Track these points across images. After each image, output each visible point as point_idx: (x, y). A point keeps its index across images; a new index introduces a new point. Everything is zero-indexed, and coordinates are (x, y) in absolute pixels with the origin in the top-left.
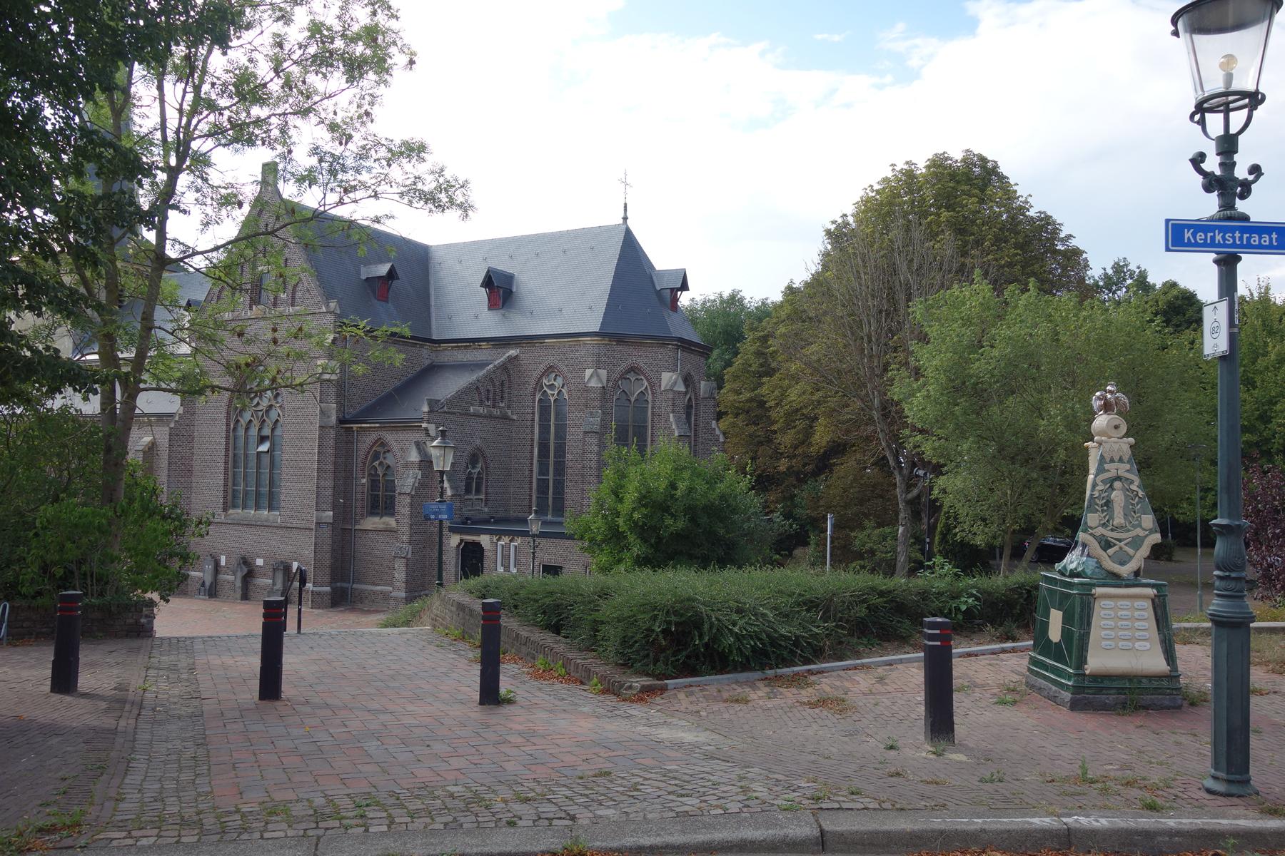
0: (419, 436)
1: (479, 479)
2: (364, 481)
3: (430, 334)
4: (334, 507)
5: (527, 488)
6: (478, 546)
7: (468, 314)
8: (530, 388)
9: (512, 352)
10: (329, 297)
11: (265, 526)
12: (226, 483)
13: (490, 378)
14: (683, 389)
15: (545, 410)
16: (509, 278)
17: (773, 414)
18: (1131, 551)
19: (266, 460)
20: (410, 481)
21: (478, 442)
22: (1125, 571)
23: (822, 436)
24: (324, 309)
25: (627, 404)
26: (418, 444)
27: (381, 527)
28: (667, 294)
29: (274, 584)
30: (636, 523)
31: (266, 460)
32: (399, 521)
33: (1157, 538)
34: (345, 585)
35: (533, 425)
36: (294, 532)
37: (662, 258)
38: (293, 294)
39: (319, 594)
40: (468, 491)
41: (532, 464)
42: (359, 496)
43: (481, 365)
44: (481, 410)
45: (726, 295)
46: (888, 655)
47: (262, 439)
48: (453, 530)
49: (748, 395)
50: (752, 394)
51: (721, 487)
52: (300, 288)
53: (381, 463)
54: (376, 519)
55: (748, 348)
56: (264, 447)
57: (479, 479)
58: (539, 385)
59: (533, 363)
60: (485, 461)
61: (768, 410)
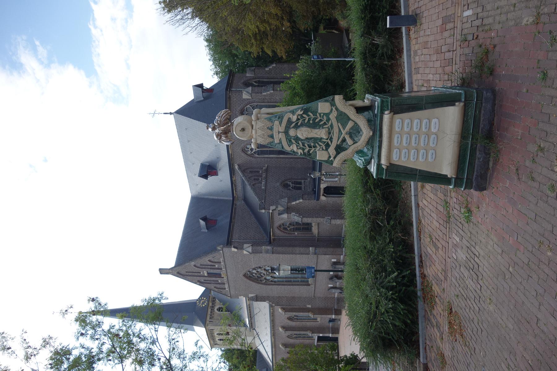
2: (296, 233)
4: (308, 246)
6: (325, 189)
7: (221, 181)
9: (236, 167)
10: (214, 250)
12: (298, 285)
13: (249, 179)
14: (250, 88)
15: (262, 153)
16: (203, 166)
18: (350, 125)
20: (296, 217)
21: (278, 184)
22: (366, 133)
26: (279, 214)
27: (316, 227)
32: (314, 222)
33: (338, 98)
35: (269, 158)
36: (319, 261)
37: (188, 96)
38: (215, 262)
40: (300, 188)
41: (288, 158)
42: (302, 235)
44: (263, 183)
45: (206, 44)
46: (413, 233)
48: (318, 199)
49: (253, 41)
50: (253, 38)
51: (298, 88)
53: (288, 227)
54: (313, 228)
59: (241, 158)
60: (287, 180)
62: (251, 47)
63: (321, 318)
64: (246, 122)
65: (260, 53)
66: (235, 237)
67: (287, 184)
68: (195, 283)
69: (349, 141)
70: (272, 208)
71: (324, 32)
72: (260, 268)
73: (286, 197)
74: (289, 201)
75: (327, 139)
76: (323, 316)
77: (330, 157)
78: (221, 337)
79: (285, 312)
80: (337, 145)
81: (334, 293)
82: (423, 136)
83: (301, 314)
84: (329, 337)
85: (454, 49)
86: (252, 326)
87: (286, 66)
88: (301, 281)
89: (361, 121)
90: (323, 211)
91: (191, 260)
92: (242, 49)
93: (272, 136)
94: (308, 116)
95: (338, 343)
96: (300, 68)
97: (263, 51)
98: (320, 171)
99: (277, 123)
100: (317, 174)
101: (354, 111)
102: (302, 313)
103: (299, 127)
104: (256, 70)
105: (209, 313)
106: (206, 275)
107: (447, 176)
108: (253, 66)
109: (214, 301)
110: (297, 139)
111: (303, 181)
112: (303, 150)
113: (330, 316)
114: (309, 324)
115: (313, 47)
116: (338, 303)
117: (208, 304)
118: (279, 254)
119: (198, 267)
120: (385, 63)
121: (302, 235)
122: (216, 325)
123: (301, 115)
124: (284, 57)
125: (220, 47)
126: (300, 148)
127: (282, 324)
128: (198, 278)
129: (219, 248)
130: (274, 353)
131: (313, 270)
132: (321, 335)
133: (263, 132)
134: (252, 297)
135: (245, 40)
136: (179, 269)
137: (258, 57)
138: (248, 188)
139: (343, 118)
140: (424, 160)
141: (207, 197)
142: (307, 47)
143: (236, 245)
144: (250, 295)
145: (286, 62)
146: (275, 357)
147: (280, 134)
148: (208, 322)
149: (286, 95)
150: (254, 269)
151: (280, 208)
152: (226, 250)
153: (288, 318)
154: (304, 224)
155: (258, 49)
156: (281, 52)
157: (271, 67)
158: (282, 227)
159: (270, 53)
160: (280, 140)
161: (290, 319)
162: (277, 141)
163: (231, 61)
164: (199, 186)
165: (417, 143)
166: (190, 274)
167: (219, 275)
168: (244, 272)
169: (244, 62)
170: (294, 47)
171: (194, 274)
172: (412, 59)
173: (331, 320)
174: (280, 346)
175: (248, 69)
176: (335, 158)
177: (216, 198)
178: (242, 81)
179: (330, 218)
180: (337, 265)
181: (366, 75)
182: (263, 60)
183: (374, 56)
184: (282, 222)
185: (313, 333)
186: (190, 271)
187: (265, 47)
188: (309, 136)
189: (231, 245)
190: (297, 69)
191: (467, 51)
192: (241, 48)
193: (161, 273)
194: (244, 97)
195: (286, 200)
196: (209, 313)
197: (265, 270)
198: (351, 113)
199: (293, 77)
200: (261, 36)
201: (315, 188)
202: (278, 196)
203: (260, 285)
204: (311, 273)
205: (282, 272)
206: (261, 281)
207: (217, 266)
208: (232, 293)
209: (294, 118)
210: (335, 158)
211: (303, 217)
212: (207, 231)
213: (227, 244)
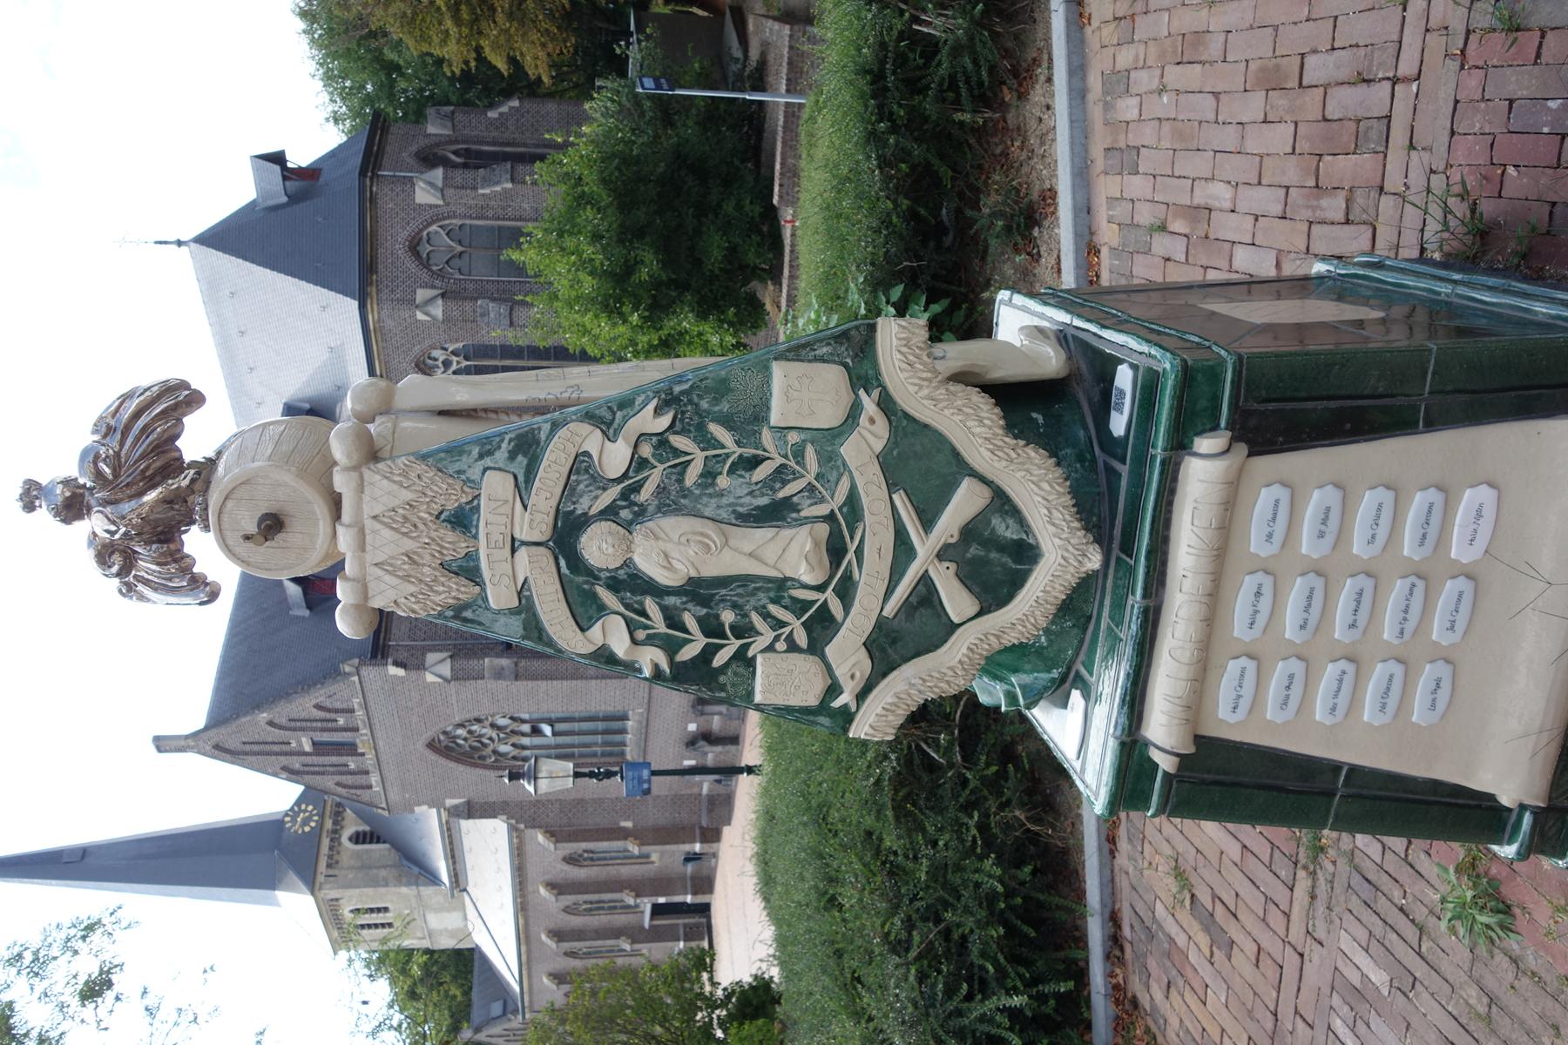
11: (646, 726)
18: (965, 502)
19: (560, 727)
22: (1062, 554)
24: (356, 678)
25: (466, 257)
28: (293, 185)
29: (720, 713)
30: (645, 319)
31: (560, 727)
37: (237, 190)
38: (337, 711)
45: (301, 25)
47: (536, 731)
49: (449, 23)
52: (328, 704)
56: (547, 729)
62: (444, 42)
63: (662, 854)
64: (288, 478)
65: (473, 64)
68: (275, 775)
69: (956, 600)
71: (666, 10)
72: (478, 720)
75: (821, 588)
76: (668, 847)
77: (833, 690)
79: (557, 842)
80: (881, 624)
81: (700, 785)
82: (1400, 587)
84: (684, 904)
85: (1407, 67)
87: (551, 107)
88: (603, 754)
89: (1038, 490)
91: (258, 707)
92: (413, 48)
93: (469, 570)
94: (708, 442)
95: (709, 918)
96: (598, 115)
97: (480, 58)
99: (497, 485)
101: (987, 411)
103: (641, 513)
104: (459, 117)
105: (325, 849)
106: (308, 748)
107: (1491, 797)
108: (448, 103)
109: (338, 814)
110: (631, 583)
112: (671, 647)
113: (687, 847)
114: (627, 871)
115: (634, 54)
116: (710, 811)
117: (321, 824)
118: (536, 679)
119: (281, 727)
120: (958, 116)
122: (349, 885)
123: (662, 442)
124: (545, 79)
126: (651, 640)
127: (547, 877)
128: (284, 760)
129: (347, 669)
130: (524, 958)
131: (646, 773)
132: (662, 900)
133: (409, 545)
134: (456, 807)
135: (423, 20)
136: (225, 735)
137: (466, 74)
139: (922, 466)
140: (1386, 718)
142: (618, 51)
143: (402, 655)
144: (450, 802)
145: (550, 95)
146: (529, 969)
147: (523, 553)
148: (320, 878)
149: (554, 198)
152: (370, 672)
155: (464, 49)
156: (537, 64)
157: (505, 109)
159: (501, 64)
160: (523, 592)
161: (571, 860)
162: (500, 596)
163: (382, 85)
165: (1362, 623)
166: (256, 748)
167: (350, 749)
168: (428, 735)
169: (422, 90)
170: (576, 52)
172: (1096, 112)
173: (691, 858)
174: (543, 937)
175: (430, 111)
176: (861, 696)
178: (414, 148)
181: (883, 163)
182: (481, 85)
183: (914, 86)
185: (638, 896)
187: (484, 43)
188: (711, 569)
189: (385, 656)
190: (587, 119)
191: (1519, 82)
192: (410, 42)
194: (418, 200)
196: (325, 849)
197: (493, 726)
198: (973, 428)
199: (572, 144)
203: (479, 771)
204: (641, 781)
205: (544, 785)
206: (482, 758)
207: (341, 721)
209: (615, 457)
210: (861, 696)
212: (307, 613)
213: (374, 656)
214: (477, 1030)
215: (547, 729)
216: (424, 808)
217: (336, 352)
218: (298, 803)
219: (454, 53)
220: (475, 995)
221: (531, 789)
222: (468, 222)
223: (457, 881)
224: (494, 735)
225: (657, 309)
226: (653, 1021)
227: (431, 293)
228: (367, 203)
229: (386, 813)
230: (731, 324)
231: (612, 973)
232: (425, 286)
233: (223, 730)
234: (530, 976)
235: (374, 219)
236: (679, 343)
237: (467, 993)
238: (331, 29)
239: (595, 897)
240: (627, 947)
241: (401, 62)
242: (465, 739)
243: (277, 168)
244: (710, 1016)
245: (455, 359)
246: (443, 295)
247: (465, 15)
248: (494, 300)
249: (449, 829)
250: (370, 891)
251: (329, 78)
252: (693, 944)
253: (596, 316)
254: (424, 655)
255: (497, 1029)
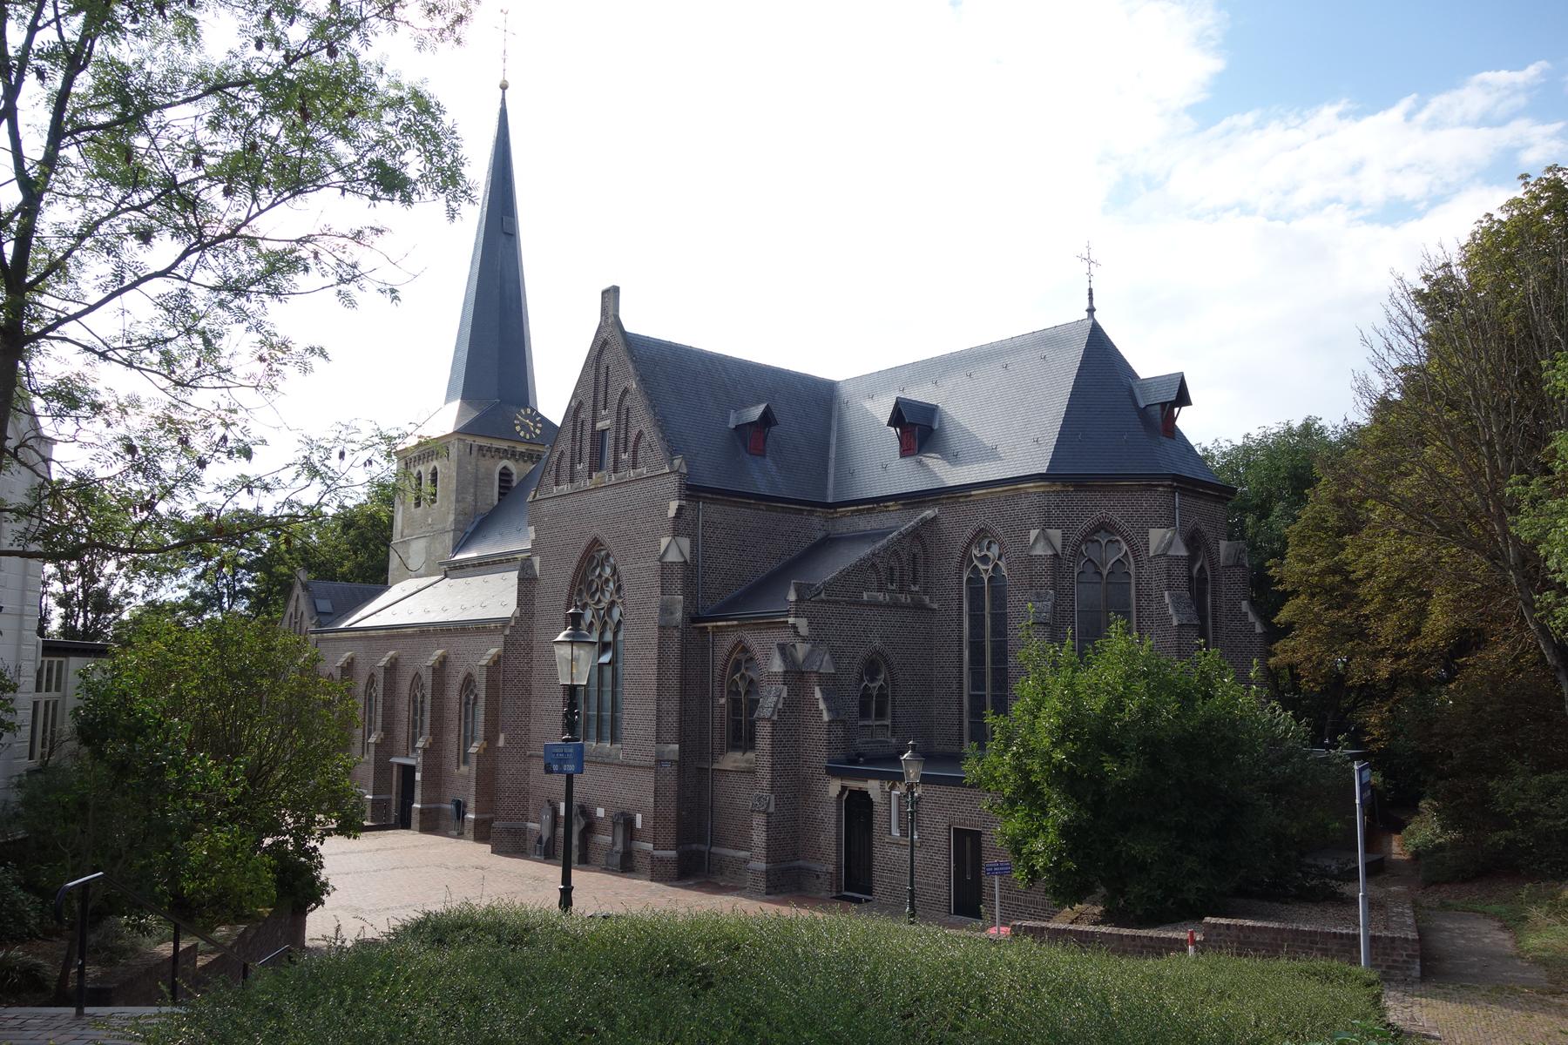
0: (784, 636)
1: (882, 696)
2: (723, 701)
3: (826, 497)
5: (955, 709)
7: (882, 467)
8: (954, 563)
9: (929, 513)
10: (672, 451)
14: (1183, 552)
16: (930, 411)
17: (1362, 591)
19: (608, 672)
21: (877, 643)
23: (1439, 620)
25: (1096, 579)
26: (782, 648)
29: (614, 843)
31: (608, 672)
32: (760, 757)
34: (702, 847)
35: (960, 614)
38: (635, 452)
39: (661, 860)
40: (864, 714)
41: (961, 672)
42: (717, 720)
43: (883, 535)
44: (880, 597)
45: (1297, 424)
48: (833, 772)
49: (1321, 564)
52: (643, 444)
54: (738, 755)
55: (1321, 495)
56: (606, 658)
57: (882, 696)
58: (966, 557)
59: (957, 526)
61: (1356, 584)
62: (1302, 559)
63: (467, 777)
65: (1280, 588)
66: (713, 512)
67: (878, 672)
68: (575, 395)
70: (803, 625)
73: (838, 669)
74: (823, 680)
76: (473, 784)
78: (426, 479)
81: (539, 821)
83: (481, 717)
86: (455, 570)
90: (792, 787)
91: (643, 380)
97: (1285, 597)
98: (925, 780)
100: (913, 772)
102: (482, 718)
105: (497, 444)
106: (599, 425)
111: (888, 722)
113: (471, 804)
114: (452, 739)
116: (508, 831)
117: (522, 441)
119: (621, 401)
121: (717, 720)
122: (460, 466)
125: (1295, 462)
128: (589, 404)
129: (677, 462)
130: (373, 633)
131: (571, 768)
132: (418, 776)
134: (532, 566)
135: (1321, 539)
136: (618, 345)
138: (865, 551)
141: (835, 428)
143: (688, 514)
144: (537, 560)
146: (360, 638)
148: (469, 440)
150: (614, 571)
151: (801, 650)
152: (672, 483)
153: (470, 675)
154: (752, 724)
155: (1295, 579)
157: (1251, 618)
158: (743, 657)
159: (1283, 615)
161: (468, 682)
164: (868, 405)
166: (602, 378)
167: (597, 465)
168: (607, 541)
171: (602, 389)
173: (460, 808)
177: (832, 455)
178: (1203, 528)
179: (772, 809)
180: (625, 831)
184: (759, 656)
185: (425, 750)
186: (612, 379)
187: (1303, 600)
189: (688, 498)
193: (604, 293)
195: (827, 668)
196: (497, 444)
197: (613, 603)
200: (1339, 589)
201: (867, 763)
202: (839, 643)
204: (561, 762)
205: (564, 652)
206: (580, 593)
207: (624, 457)
208: (546, 505)
211: (774, 723)
213: (689, 487)
214: (305, 587)
215: (606, 658)
216: (533, 536)
217: (991, 454)
218: (544, 420)
219: (1291, 569)
220: (339, 584)
221: (560, 638)
222: (1133, 581)
223: (456, 568)
224: (602, 605)
225: (1069, 781)
226: (291, 768)
227: (1058, 544)
228: (1148, 482)
229: (530, 499)
230: (1057, 864)
231: (346, 723)
232: (1064, 538)
233: (621, 348)
234: (353, 639)
235: (1129, 489)
236: (1030, 806)
237: (344, 578)
238: (1297, 452)
239: (428, 707)
240: (372, 740)
241: (1271, 519)
242: (600, 576)
243: (1173, 398)
244: (288, 832)
245: (990, 567)
246: (1056, 555)
247: (1328, 580)
248: (1054, 606)
249: (508, 561)
250: (453, 486)
251: (1246, 450)
252: (368, 813)
253: (1059, 714)
254: (689, 535)
255: (303, 606)
